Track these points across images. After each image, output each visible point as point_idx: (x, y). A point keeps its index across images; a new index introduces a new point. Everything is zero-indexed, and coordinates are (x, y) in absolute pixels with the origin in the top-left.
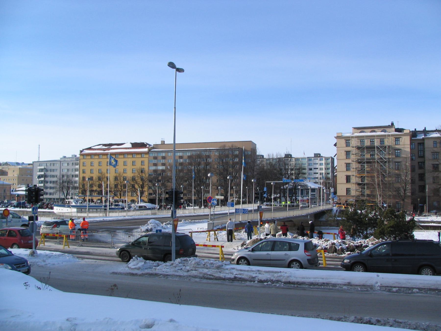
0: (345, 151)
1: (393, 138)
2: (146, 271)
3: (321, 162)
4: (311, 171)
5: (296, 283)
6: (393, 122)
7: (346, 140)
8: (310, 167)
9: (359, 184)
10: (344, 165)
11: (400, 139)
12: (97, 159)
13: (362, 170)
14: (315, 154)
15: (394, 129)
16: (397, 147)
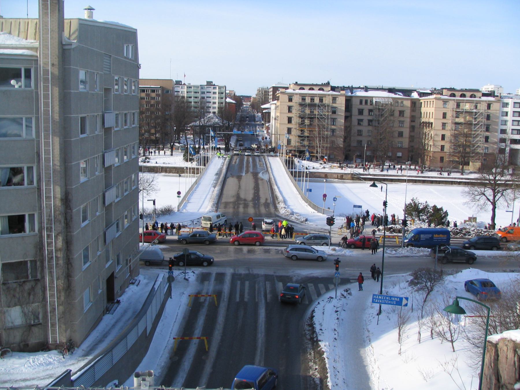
1: (331, 98)
4: (203, 95)
7: (289, 96)
8: (203, 90)
9: (299, 136)
13: (302, 123)
15: (329, 88)
16: (334, 105)
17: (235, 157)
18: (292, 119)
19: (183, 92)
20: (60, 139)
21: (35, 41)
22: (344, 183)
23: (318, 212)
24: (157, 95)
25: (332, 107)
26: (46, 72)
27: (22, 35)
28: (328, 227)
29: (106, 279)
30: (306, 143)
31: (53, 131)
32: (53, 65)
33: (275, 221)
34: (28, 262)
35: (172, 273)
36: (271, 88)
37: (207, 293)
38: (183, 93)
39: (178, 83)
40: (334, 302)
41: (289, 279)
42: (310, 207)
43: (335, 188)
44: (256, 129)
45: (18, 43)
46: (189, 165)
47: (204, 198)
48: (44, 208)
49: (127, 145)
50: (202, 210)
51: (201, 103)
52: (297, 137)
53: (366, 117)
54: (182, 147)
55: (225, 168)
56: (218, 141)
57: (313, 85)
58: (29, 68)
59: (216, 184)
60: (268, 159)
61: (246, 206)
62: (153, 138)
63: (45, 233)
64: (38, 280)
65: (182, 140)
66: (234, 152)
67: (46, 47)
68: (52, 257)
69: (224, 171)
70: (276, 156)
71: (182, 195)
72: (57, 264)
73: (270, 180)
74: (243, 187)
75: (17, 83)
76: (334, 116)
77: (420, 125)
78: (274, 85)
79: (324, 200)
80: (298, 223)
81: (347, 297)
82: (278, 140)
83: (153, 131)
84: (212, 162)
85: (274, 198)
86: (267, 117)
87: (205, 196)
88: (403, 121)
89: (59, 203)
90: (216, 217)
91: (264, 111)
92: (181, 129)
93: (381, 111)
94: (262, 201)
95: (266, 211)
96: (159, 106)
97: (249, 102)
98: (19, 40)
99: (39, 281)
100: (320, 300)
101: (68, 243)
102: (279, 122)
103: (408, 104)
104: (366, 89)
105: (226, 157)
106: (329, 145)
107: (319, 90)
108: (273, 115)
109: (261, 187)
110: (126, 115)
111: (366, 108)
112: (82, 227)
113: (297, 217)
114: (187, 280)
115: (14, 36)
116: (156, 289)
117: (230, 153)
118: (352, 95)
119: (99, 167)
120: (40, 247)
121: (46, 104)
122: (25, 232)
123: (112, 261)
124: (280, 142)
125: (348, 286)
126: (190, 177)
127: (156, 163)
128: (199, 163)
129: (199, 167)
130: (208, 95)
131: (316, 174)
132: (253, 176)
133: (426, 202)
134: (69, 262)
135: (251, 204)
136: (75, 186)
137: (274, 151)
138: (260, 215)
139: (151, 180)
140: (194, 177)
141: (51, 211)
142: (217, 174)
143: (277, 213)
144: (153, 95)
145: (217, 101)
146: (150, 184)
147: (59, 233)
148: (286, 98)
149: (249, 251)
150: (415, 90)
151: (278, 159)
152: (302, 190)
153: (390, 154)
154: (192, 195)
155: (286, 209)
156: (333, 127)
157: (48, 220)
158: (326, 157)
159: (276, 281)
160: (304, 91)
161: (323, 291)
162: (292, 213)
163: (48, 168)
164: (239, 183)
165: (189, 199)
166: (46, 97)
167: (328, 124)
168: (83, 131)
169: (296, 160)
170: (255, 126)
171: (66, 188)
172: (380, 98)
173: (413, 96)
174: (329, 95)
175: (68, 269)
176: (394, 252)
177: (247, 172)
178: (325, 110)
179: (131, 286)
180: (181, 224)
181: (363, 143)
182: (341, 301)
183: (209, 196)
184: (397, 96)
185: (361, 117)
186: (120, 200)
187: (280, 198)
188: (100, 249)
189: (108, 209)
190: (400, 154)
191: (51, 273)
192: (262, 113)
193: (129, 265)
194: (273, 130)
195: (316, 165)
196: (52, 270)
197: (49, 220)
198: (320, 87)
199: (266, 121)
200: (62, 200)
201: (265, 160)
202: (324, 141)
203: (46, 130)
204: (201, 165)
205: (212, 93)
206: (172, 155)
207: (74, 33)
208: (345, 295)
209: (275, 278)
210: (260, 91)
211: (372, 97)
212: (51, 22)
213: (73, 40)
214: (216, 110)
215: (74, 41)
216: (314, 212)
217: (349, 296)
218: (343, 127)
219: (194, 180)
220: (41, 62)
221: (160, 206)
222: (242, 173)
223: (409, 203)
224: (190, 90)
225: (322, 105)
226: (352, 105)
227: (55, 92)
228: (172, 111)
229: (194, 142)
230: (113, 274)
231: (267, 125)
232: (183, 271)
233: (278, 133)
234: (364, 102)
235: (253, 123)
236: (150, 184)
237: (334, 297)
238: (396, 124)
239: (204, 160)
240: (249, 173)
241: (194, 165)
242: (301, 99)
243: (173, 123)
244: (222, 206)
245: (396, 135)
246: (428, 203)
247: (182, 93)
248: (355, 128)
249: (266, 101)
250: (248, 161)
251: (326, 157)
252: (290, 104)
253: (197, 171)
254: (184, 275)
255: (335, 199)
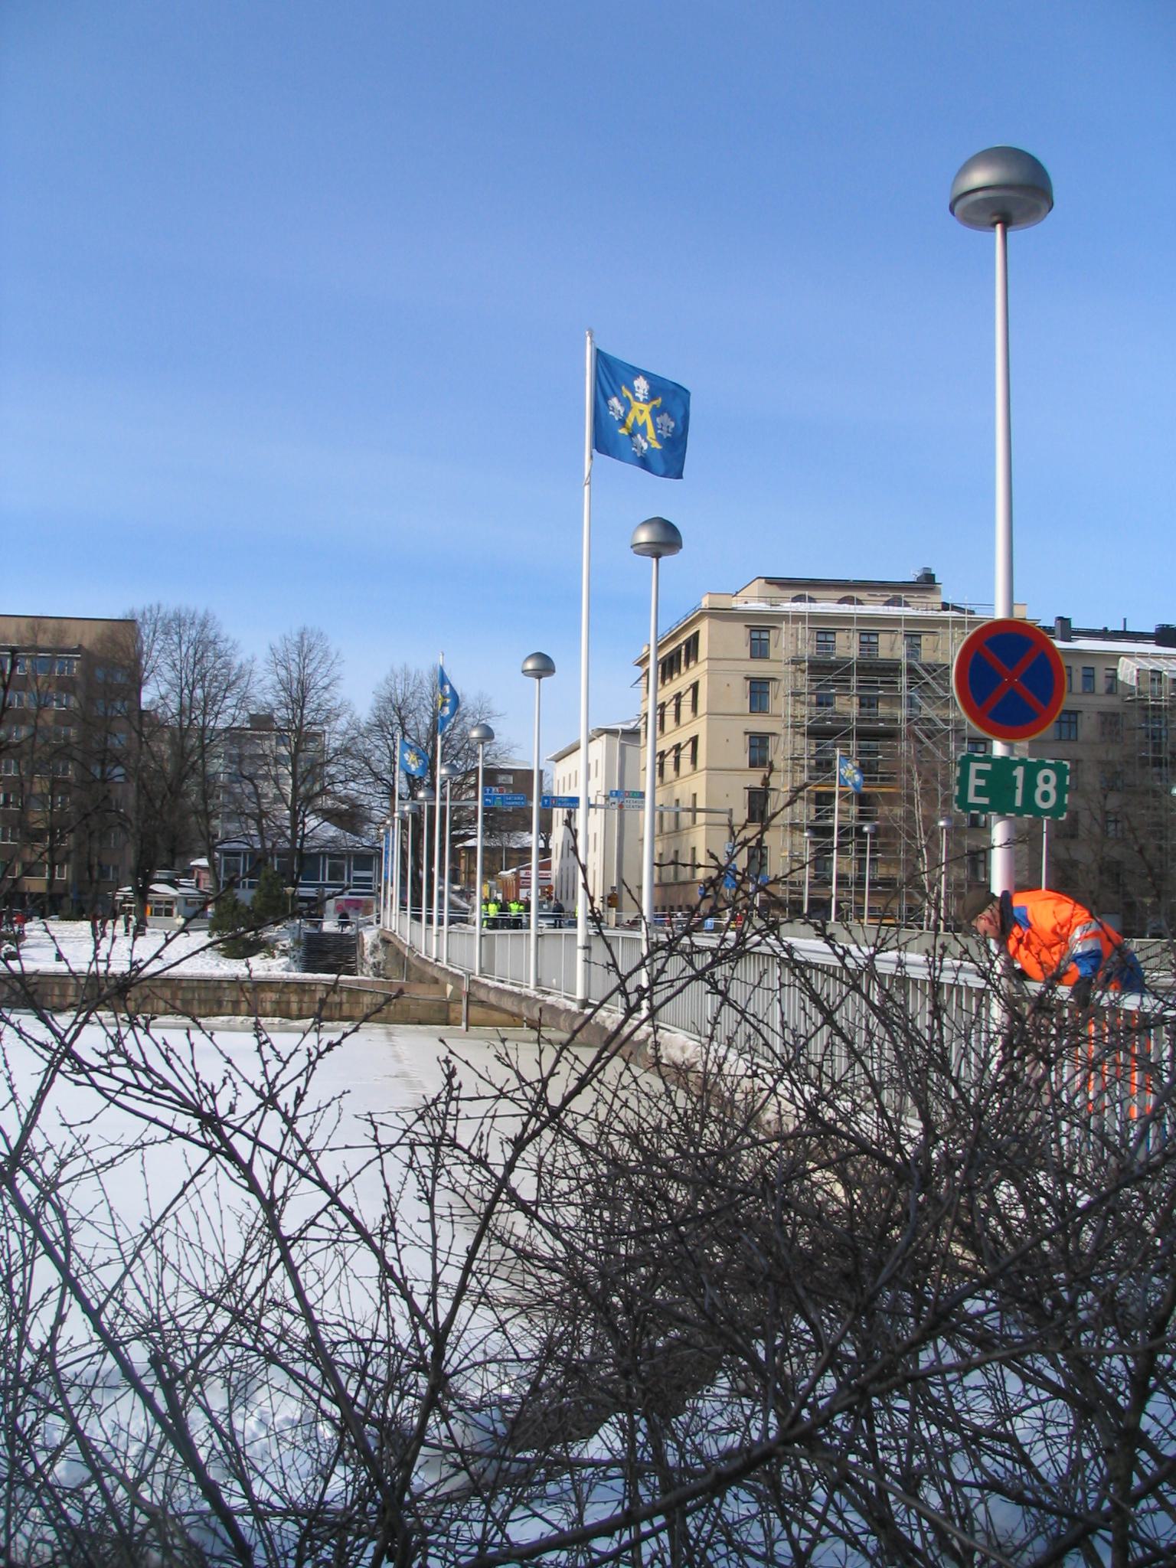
0: (747, 678)
5: (1060, 874)
7: (753, 629)
10: (743, 743)
12: (271, 1486)
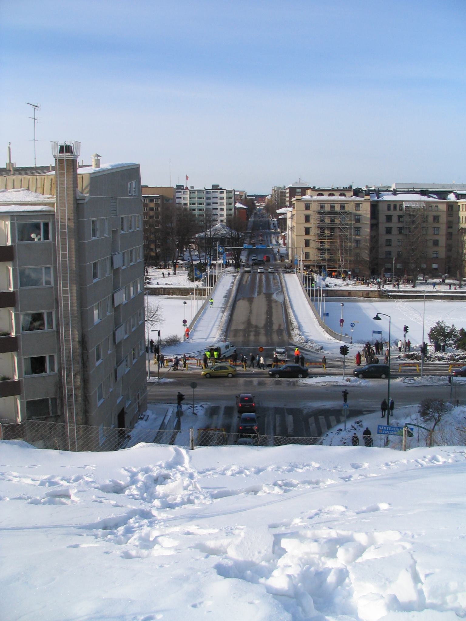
1: (353, 204)
2: (414, 385)
3: (222, 195)
4: (209, 201)
6: (351, 185)
7: (306, 204)
8: (209, 195)
9: (319, 249)
11: (361, 205)
13: (322, 235)
14: (213, 186)
15: (352, 193)
16: (358, 212)
17: (246, 275)
18: (310, 229)
19: (185, 199)
20: (76, 287)
21: (51, 196)
22: (371, 301)
23: (336, 338)
24: (156, 205)
25: (356, 215)
26: (63, 226)
27: (39, 190)
28: (342, 356)
29: (117, 414)
30: (327, 256)
31: (71, 281)
32: (69, 219)
33: (287, 350)
34: (50, 399)
35: (181, 407)
36: (287, 188)
37: (216, 427)
38: (185, 199)
39: (180, 188)
40: (343, 434)
41: (299, 411)
42: (326, 333)
43: (360, 308)
44: (271, 238)
45: (36, 199)
46: (194, 285)
47: (212, 325)
48: (63, 350)
49: (133, 281)
50: (209, 340)
51: (207, 215)
52: (316, 250)
53: (395, 225)
54: (185, 264)
55: (234, 288)
56: (227, 256)
57: (333, 190)
58: (47, 222)
59: (225, 308)
60: (284, 277)
61: (257, 334)
62: (153, 254)
63: (65, 373)
64: (58, 416)
65: (187, 254)
66: (246, 269)
67: (63, 204)
68: (72, 395)
69: (234, 292)
70: (293, 273)
71: (188, 324)
72: (76, 401)
73: (284, 303)
74: (254, 312)
75: (37, 237)
76: (358, 225)
77: (459, 230)
78: (291, 186)
79: (342, 326)
80: (312, 352)
81: (357, 429)
82: (294, 254)
83: (153, 246)
84: (220, 282)
85: (289, 323)
86: (282, 223)
87: (213, 322)
88: (438, 228)
89: (77, 346)
90: (224, 347)
91: (280, 217)
92: (184, 243)
93: (412, 217)
94: (275, 327)
95: (279, 338)
96: (158, 218)
97: (264, 203)
98: (37, 196)
99: (60, 417)
100: (329, 433)
101: (85, 381)
102: (295, 233)
103: (443, 207)
104: (395, 192)
105: (236, 276)
106: (353, 258)
107: (341, 195)
108: (289, 222)
109: (274, 311)
110: (131, 251)
111: (395, 214)
112: (96, 366)
113: (312, 345)
114: (195, 414)
115: (32, 192)
116: (166, 424)
117: (241, 270)
118: (378, 200)
119: (109, 308)
120: (59, 386)
121: (64, 256)
122: (46, 372)
123: (122, 397)
124: (297, 257)
125: (360, 418)
126: (196, 299)
127: (158, 284)
128: (206, 283)
129: (206, 287)
130: (215, 200)
131: (339, 292)
132: (266, 297)
133: (453, 325)
134: (86, 399)
135: (262, 331)
136: (90, 329)
137: (290, 268)
138: (272, 344)
139: (155, 310)
140: (201, 299)
141: (70, 352)
142: (226, 297)
143: (290, 341)
144: (152, 205)
145: (225, 207)
146: (154, 315)
147: (78, 373)
148: (302, 206)
149: (260, 384)
150: (452, 192)
151: (295, 276)
152: (319, 313)
153: (424, 266)
154: (198, 322)
155: (300, 337)
156: (357, 237)
157: (67, 361)
158: (349, 273)
159: (286, 414)
160: (322, 197)
161: (333, 423)
162: (307, 341)
163: (66, 313)
164: (251, 307)
165: (196, 327)
166: (64, 249)
167: (351, 235)
168: (95, 276)
169: (316, 277)
170: (270, 234)
171: (82, 331)
172: (411, 202)
173: (450, 199)
174: (351, 201)
175: (85, 406)
176: (412, 381)
177: (259, 293)
178: (348, 218)
179: (140, 422)
180: (187, 356)
181: (392, 254)
182: (350, 433)
183: (217, 323)
184: (431, 199)
185: (389, 225)
186: (129, 336)
187: (295, 324)
188: (112, 386)
189: (117, 346)
190: (435, 266)
191: (70, 410)
192: (278, 220)
193: (137, 401)
194: (289, 241)
195: (339, 282)
196: (72, 407)
197: (68, 362)
198: (341, 192)
199: (281, 229)
200: (79, 342)
201: (280, 277)
202: (346, 253)
203: (65, 279)
204: (207, 286)
205: (219, 198)
206: (175, 274)
207: (86, 187)
208: (355, 427)
209: (285, 411)
210: (275, 192)
211: (402, 202)
212: (67, 180)
213: (86, 194)
214: (224, 218)
215: (86, 195)
216: (331, 339)
217: (359, 428)
218: (368, 238)
219: (201, 303)
220: (59, 217)
221: (164, 336)
222: (254, 294)
223: (435, 327)
224: (193, 195)
225: (344, 213)
226: (378, 211)
227: (70, 244)
228: (174, 224)
229: (200, 258)
230: (123, 409)
231: (283, 234)
232: (191, 405)
233: (294, 246)
234: (392, 207)
235: (267, 231)
236: (154, 315)
237: (344, 429)
238: (430, 231)
239: (212, 280)
240: (262, 294)
241: (199, 284)
242: (320, 206)
243: (175, 238)
244: (231, 334)
245: (430, 244)
246: (455, 326)
247: (184, 200)
248: (383, 238)
249: (282, 205)
250: (261, 280)
251: (349, 273)
252: (308, 213)
253: (203, 293)
254: (193, 409)
255: (352, 325)
